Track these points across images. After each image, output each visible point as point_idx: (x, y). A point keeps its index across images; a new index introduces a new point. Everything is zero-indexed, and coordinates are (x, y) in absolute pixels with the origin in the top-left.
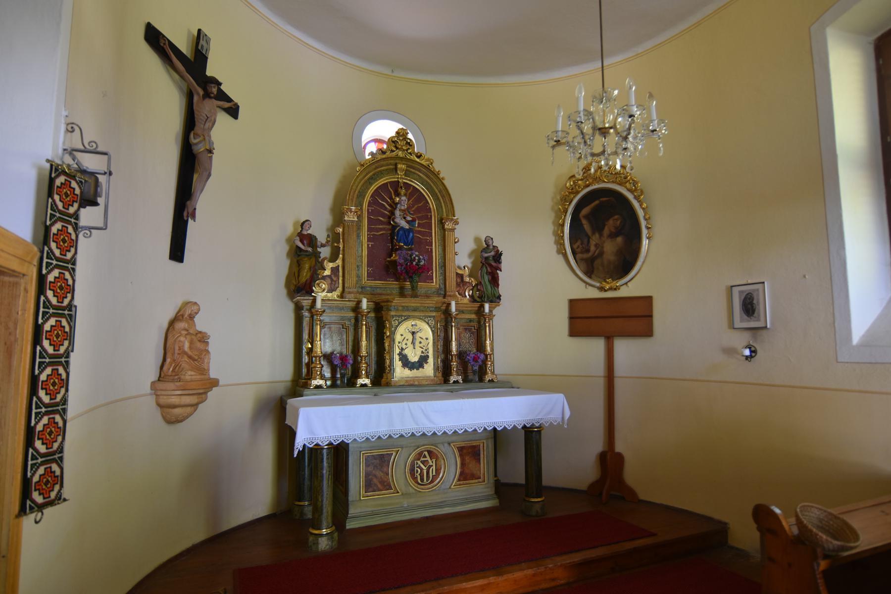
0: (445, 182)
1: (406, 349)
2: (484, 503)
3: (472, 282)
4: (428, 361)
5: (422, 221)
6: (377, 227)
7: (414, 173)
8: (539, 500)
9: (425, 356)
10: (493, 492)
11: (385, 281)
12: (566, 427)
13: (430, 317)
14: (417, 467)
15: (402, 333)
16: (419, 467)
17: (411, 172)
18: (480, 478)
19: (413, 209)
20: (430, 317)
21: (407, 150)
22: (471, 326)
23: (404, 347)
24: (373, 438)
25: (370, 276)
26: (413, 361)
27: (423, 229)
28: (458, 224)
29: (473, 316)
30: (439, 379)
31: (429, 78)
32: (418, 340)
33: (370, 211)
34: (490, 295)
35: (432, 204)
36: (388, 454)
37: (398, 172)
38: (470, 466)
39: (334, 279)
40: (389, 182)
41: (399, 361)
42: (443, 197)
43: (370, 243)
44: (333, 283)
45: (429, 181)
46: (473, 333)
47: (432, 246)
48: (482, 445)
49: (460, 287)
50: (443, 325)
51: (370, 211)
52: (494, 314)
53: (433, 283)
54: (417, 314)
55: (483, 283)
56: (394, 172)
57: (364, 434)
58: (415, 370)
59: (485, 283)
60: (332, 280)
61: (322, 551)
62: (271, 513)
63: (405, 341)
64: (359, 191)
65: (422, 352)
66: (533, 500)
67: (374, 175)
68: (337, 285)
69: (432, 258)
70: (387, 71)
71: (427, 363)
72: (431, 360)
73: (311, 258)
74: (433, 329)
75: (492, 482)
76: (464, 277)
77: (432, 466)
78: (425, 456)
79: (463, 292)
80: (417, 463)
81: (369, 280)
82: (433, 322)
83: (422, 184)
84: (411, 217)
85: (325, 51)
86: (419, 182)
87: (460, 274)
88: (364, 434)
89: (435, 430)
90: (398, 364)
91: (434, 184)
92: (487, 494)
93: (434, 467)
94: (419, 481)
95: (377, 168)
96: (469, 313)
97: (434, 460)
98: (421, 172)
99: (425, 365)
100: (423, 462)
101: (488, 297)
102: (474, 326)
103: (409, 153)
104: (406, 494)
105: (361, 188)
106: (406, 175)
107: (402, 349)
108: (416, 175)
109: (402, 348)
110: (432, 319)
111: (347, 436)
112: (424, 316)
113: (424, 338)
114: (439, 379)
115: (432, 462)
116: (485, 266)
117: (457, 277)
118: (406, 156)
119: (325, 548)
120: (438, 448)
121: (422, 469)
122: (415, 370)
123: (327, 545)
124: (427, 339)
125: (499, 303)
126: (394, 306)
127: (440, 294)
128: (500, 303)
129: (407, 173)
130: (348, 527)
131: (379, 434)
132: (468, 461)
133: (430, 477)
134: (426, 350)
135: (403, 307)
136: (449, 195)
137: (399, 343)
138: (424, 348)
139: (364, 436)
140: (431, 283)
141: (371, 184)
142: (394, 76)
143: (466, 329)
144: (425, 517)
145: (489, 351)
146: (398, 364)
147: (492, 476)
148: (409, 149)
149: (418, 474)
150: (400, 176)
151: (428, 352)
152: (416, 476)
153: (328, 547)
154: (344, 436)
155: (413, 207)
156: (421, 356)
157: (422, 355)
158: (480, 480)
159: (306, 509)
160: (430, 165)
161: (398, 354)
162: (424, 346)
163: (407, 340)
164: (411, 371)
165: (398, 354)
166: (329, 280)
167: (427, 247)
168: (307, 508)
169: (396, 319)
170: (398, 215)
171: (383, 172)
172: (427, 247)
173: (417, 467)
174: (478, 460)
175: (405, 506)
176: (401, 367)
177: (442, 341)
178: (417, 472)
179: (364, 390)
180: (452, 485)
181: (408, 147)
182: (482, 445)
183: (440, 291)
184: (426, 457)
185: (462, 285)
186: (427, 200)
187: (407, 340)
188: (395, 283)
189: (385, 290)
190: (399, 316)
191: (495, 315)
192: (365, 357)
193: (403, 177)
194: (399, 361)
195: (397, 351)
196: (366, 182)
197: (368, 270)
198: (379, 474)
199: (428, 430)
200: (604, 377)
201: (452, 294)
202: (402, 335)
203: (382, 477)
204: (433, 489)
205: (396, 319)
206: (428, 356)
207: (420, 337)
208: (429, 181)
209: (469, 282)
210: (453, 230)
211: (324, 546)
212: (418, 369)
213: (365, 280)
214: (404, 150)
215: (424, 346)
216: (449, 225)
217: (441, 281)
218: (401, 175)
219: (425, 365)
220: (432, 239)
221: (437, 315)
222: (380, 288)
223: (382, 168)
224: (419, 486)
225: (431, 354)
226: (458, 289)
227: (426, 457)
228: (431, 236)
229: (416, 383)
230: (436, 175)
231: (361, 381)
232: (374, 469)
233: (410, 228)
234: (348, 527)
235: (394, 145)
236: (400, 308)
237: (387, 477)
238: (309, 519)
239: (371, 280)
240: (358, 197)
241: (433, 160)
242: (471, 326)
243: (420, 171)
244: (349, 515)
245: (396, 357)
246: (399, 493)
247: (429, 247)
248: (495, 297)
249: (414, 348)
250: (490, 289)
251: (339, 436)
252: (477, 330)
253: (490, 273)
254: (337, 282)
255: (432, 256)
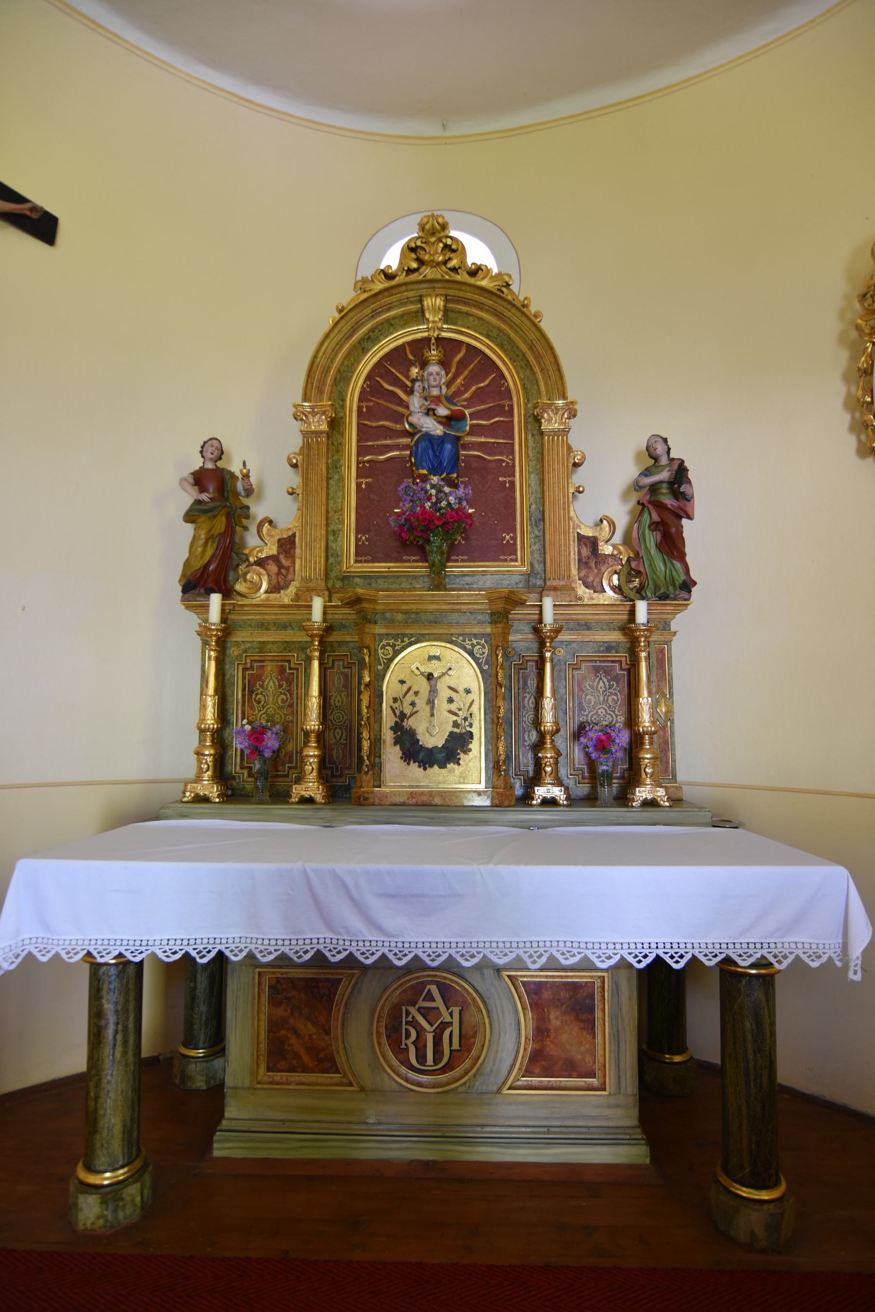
0: (543, 325)
1: (411, 715)
2: (605, 1149)
3: (620, 553)
4: (470, 746)
5: (489, 420)
6: (379, 443)
7: (467, 314)
8: (765, 1195)
9: (461, 735)
10: (635, 1122)
11: (397, 561)
12: (858, 978)
13: (475, 636)
14: (407, 1023)
15: (402, 677)
16: (414, 1023)
17: (460, 312)
18: (592, 1075)
19: (467, 395)
20: (475, 636)
21: (445, 263)
22: (613, 662)
23: (408, 710)
24: (204, 956)
25: (361, 552)
26: (430, 746)
27: (493, 437)
28: (575, 416)
29: (615, 636)
30: (498, 794)
31: (525, 119)
32: (444, 693)
33: (364, 410)
34: (661, 582)
35: (512, 376)
36: (328, 980)
37: (427, 316)
38: (564, 1037)
39: (285, 562)
40: (408, 343)
41: (395, 744)
42: (538, 357)
43: (364, 480)
44: (283, 571)
45: (503, 326)
46: (616, 678)
47: (513, 475)
48: (598, 984)
49: (589, 568)
50: (536, 658)
51: (364, 410)
52: (673, 629)
53: (516, 560)
54: (441, 631)
55: (642, 553)
56: (420, 318)
57: (178, 942)
58: (436, 767)
59: (648, 551)
60: (280, 566)
61: (86, 1229)
62: (150, 1055)
63: (410, 697)
64: (339, 370)
65: (456, 724)
66: (745, 1192)
67: (372, 330)
68: (290, 577)
69: (515, 503)
70: (429, 128)
71: (467, 751)
72: (478, 748)
73: (214, 517)
74: (486, 667)
75: (630, 1091)
76: (601, 544)
77: (450, 1024)
78: (430, 997)
79: (597, 580)
80: (408, 1013)
81: (360, 562)
82: (486, 651)
83: (488, 336)
84: (448, 408)
85: (291, 111)
86: (480, 333)
87: (588, 538)
88: (178, 942)
89: (386, 951)
90: (392, 754)
91: (516, 332)
92: (612, 1124)
93: (456, 1028)
94: (414, 1061)
95: (375, 314)
96: (603, 629)
97: (456, 1010)
98: (482, 309)
99: (462, 756)
100: (425, 1013)
101: (657, 587)
102: (621, 662)
103: (450, 269)
104: (373, 1091)
105: (342, 364)
106: (446, 319)
107: (403, 716)
108: (471, 319)
109: (402, 712)
110: (483, 641)
111: (131, 943)
112: (460, 635)
113: (461, 689)
114: (498, 794)
115: (451, 1014)
116: (648, 509)
117: (579, 544)
118: (442, 276)
119: (93, 1223)
120: (466, 981)
121: (420, 1031)
122: (436, 767)
123: (98, 1218)
124: (468, 691)
125: (688, 599)
126: (384, 613)
127: (535, 586)
128: (691, 600)
129: (448, 315)
130: (216, 1153)
131: (219, 947)
132: (559, 1023)
133: (442, 1054)
134: (465, 719)
135: (406, 612)
136: (551, 349)
137: (395, 700)
138: (460, 713)
139: (176, 948)
140: (511, 560)
141: (365, 351)
142: (449, 137)
143: (596, 670)
144: (421, 1161)
145: (647, 724)
146: (392, 754)
147: (629, 1074)
148: (450, 259)
149: (409, 1042)
150: (430, 325)
151: (471, 725)
152: (403, 1046)
153: (101, 1222)
154: (125, 943)
155: (466, 391)
156: (451, 733)
157: (456, 730)
158: (593, 1081)
159: (192, 1066)
160: (504, 289)
161: (392, 728)
162: (460, 709)
163: (416, 693)
164: (425, 769)
165: (392, 728)
166: (273, 568)
167: (501, 479)
168: (194, 1066)
169: (388, 644)
170: (417, 405)
171: (393, 322)
172: (501, 479)
173: (407, 1023)
174: (589, 1026)
175: (371, 1121)
176: (400, 760)
177: (532, 699)
178: (408, 1035)
179: (305, 810)
180: (504, 1083)
181: (449, 255)
182: (598, 984)
183: (532, 580)
184: (433, 1000)
185: (593, 564)
186: (501, 372)
187: (416, 693)
188: (420, 564)
189: (398, 581)
190: (396, 637)
191: (675, 633)
192: (652, 734)
193: (440, 325)
194: (395, 744)
195: (388, 719)
196: (353, 348)
197: (357, 540)
198: (307, 1028)
199: (364, 949)
200: (634, 1095)
201: (562, 583)
202: (402, 682)
203: (314, 1037)
204: (447, 1088)
205: (388, 644)
206: (471, 735)
207: (450, 687)
208: (503, 326)
209: (612, 555)
210: (565, 432)
211: (92, 1217)
212: (442, 766)
213: (350, 563)
214: (438, 264)
215: (460, 709)
216: (551, 423)
217: (537, 556)
218: (434, 322)
219: (462, 756)
220: (513, 460)
221: (495, 631)
222: (385, 577)
223: (392, 313)
224: (412, 1075)
225: (479, 729)
226: (583, 574)
227: (433, 999)
228: (512, 453)
229: (438, 800)
230: (521, 308)
231: (298, 790)
232: (292, 1014)
233: (445, 433)
234: (216, 1153)
235: (414, 256)
236: (400, 617)
237: (327, 1038)
238: (198, 1091)
239: (366, 561)
240: (336, 382)
241: (510, 276)
242: (613, 662)
243: (480, 306)
244: (224, 1122)
245: (388, 736)
246: (352, 1085)
247: (507, 479)
248: (674, 585)
249: (432, 715)
250: (663, 568)
251: (112, 942)
252: (629, 671)
253: (657, 523)
254: (292, 569)
255: (514, 498)
